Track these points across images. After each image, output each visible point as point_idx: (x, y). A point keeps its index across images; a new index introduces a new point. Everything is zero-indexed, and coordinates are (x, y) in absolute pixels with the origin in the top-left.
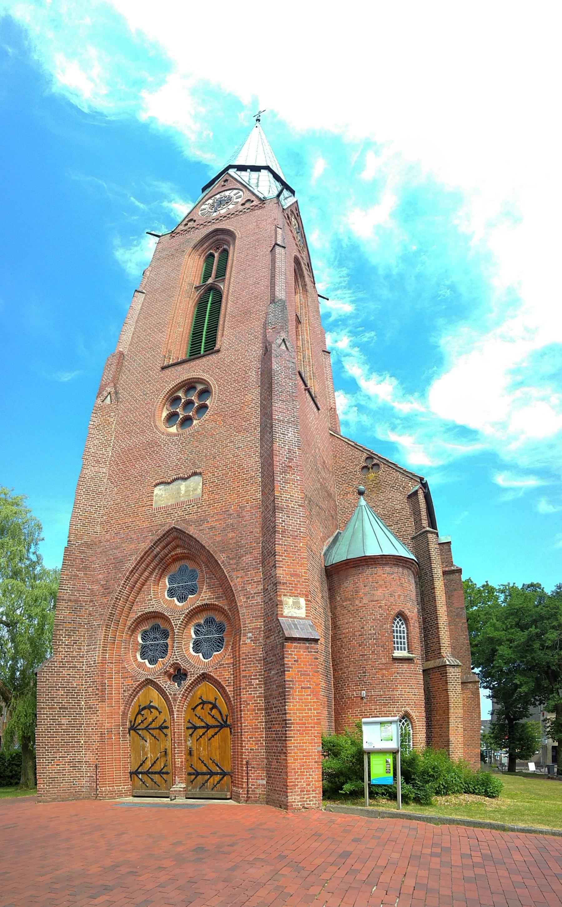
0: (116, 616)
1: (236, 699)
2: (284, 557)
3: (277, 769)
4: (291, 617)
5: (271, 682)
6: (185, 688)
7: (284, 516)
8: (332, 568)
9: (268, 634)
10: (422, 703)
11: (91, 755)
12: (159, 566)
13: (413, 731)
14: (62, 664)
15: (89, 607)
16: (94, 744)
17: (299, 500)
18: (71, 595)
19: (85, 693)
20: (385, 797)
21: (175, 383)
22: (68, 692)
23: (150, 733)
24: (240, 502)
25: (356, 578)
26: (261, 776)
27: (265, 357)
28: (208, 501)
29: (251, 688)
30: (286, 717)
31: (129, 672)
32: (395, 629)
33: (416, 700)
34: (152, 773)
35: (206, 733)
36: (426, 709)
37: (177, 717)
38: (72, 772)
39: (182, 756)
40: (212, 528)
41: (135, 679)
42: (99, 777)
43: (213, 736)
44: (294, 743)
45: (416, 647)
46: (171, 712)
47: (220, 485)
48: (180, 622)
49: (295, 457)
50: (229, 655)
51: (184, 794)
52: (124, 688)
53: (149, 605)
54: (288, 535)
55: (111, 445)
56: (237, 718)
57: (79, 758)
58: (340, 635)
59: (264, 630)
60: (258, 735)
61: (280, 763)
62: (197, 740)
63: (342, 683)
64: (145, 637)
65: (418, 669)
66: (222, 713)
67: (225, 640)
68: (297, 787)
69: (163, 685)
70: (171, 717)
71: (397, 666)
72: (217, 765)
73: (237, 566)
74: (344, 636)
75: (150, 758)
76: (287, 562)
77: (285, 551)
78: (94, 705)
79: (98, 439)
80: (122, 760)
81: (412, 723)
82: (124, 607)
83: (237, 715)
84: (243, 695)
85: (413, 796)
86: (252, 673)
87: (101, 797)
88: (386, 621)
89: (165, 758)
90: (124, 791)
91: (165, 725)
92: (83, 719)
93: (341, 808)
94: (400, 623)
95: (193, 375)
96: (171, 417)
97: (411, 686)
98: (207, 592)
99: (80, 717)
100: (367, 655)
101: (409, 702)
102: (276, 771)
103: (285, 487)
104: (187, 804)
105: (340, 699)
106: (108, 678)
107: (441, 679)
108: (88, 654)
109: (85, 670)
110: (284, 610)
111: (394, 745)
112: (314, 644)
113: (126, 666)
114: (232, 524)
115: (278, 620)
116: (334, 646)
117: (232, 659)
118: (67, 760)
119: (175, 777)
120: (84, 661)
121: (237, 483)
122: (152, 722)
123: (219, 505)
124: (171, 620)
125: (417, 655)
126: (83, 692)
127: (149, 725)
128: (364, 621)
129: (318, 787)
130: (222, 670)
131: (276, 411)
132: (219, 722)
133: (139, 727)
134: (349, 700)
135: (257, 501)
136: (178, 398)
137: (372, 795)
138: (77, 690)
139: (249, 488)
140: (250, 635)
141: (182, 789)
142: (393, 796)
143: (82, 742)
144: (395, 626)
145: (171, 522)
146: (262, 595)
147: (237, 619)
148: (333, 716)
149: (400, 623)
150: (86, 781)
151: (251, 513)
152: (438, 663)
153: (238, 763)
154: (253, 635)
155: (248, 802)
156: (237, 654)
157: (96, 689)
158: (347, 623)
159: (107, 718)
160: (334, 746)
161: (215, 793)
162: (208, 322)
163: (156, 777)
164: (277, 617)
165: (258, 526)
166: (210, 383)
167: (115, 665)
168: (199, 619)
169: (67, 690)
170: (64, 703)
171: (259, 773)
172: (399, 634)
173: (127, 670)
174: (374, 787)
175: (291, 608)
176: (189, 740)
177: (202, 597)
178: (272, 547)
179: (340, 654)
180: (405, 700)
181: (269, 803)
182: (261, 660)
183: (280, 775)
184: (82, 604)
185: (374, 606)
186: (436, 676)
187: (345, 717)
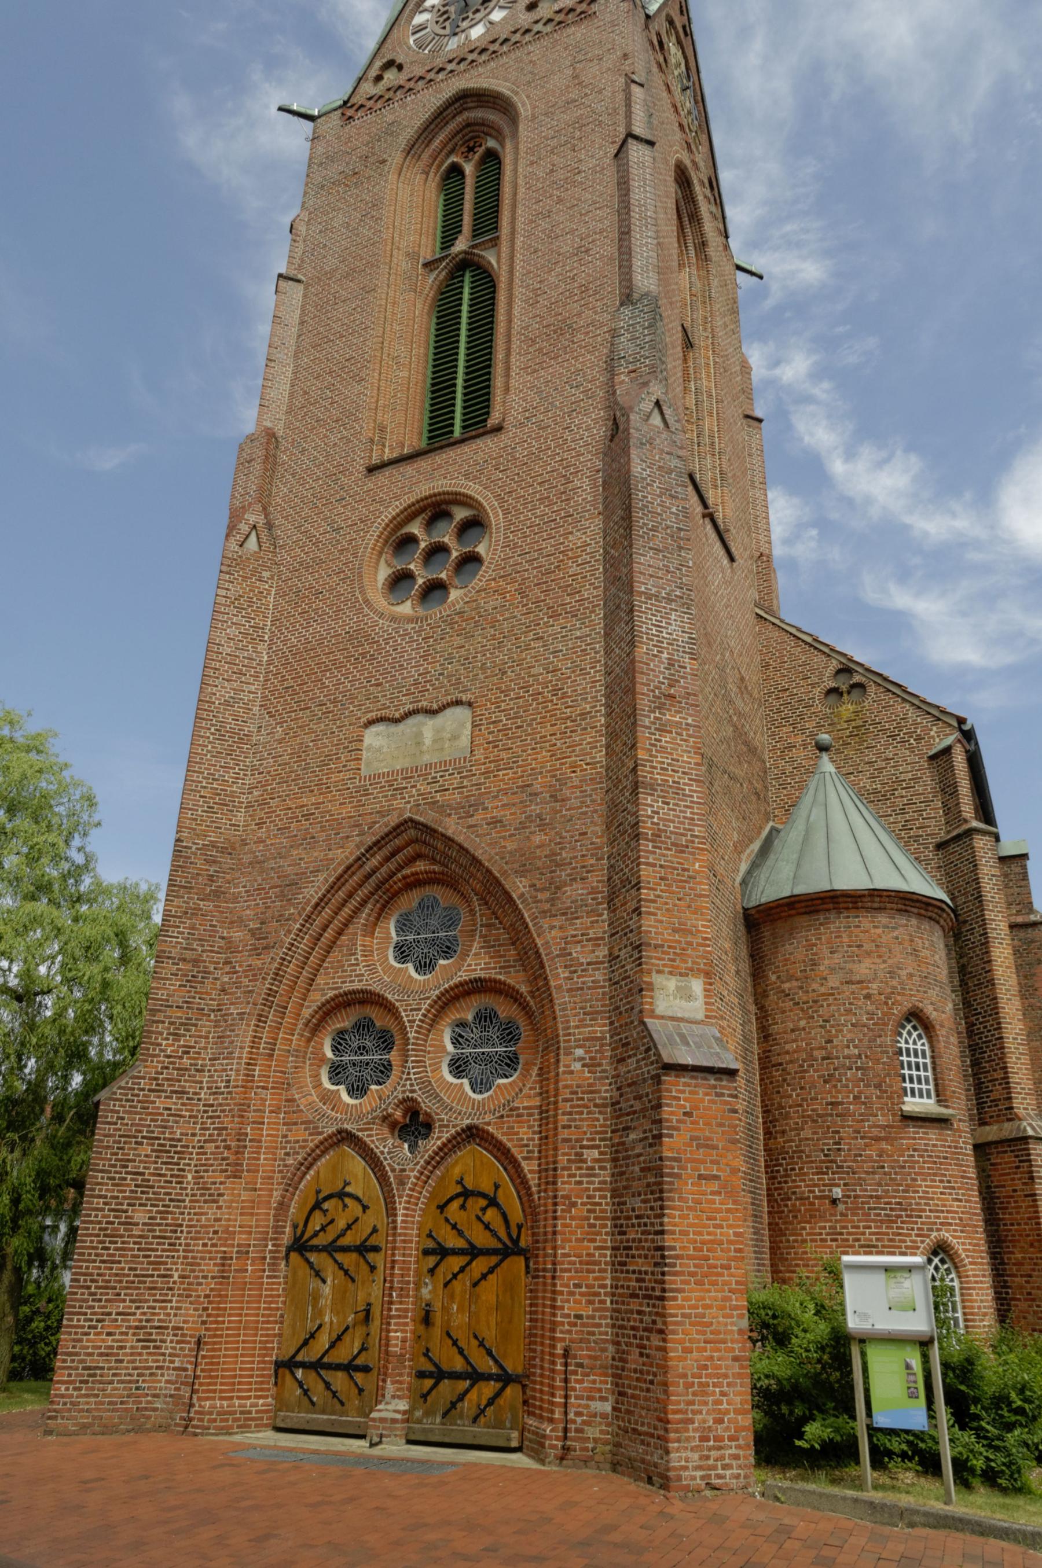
0: (281, 995)
1: (545, 1191)
2: (658, 893)
3: (641, 1372)
4: (672, 1019)
5: (628, 1157)
6: (426, 1157)
7: (658, 802)
8: (758, 912)
9: (621, 1053)
10: (977, 1221)
11: (191, 1312)
12: (376, 897)
13: (961, 1283)
14: (157, 1085)
15: (222, 974)
17: (692, 769)
18: (186, 949)
19: (198, 1154)
20: (910, 1465)
21: (401, 504)
23: (336, 1261)
24: (557, 770)
25: (813, 935)
26: (600, 1390)
27: (613, 446)
28: (485, 763)
29: (580, 1168)
30: (663, 1240)
31: (301, 1111)
32: (903, 1045)
33: (963, 1213)
34: (329, 1367)
35: (468, 1269)
36: (988, 1236)
37: (403, 1221)
38: (140, 1354)
39: (406, 1324)
40: (497, 822)
41: (314, 1128)
42: (202, 1370)
43: (484, 1277)
44: (683, 1307)
45: (954, 1092)
46: (391, 1212)
47: (511, 729)
48: (420, 1017)
49: (683, 677)
50: (531, 1089)
51: (403, 1428)
52: (286, 1148)
53: (351, 976)
54: (666, 843)
55: (266, 638)
56: (545, 1234)
57: (162, 1317)
58: (778, 1055)
59: (610, 1044)
61: (648, 1356)
62: (446, 1285)
63: (787, 1164)
64: (341, 1044)
65: (964, 1142)
66: (509, 1218)
67: (521, 1061)
68: (690, 1426)
69: (377, 1148)
70: (390, 1219)
71: (915, 1133)
72: (489, 1353)
73: (552, 905)
74: (787, 1057)
75: (328, 1326)
76: (666, 903)
77: (661, 878)
78: (215, 1183)
79: (236, 624)
80: (262, 1329)
81: (956, 1267)
82: (298, 978)
83: (545, 1226)
84: (563, 1183)
85: (979, 1464)
86: (585, 1133)
88: (882, 1030)
89: (364, 1328)
90: (257, 1412)
91: (372, 1242)
92: (183, 1213)
93: (803, 1492)
94: (915, 1034)
95: (442, 484)
96: (400, 579)
97: (949, 1182)
98: (480, 954)
99: (178, 1207)
100: (842, 1103)
101: (946, 1218)
102: (638, 1380)
103: (660, 741)
104: (413, 1461)
105: (782, 1200)
106: (254, 1122)
107: (1018, 1167)
108: (213, 1065)
109: (205, 1099)
110: (658, 1003)
111: (920, 1323)
112: (728, 1081)
113: (297, 1096)
114: (539, 816)
115: (644, 1024)
116: (768, 1081)
117: (538, 1099)
118: (134, 1321)
119: (384, 1381)
120: (205, 1080)
121: (552, 725)
123: (507, 774)
124: (401, 1009)
125: (958, 1109)
126: (195, 1151)
128: (832, 1026)
129: (744, 1428)
130: (514, 1122)
131: (641, 573)
132: (499, 1239)
134: (804, 1205)
135: (595, 768)
136: (410, 540)
137: (880, 1458)
138: (182, 1146)
139: (577, 739)
140: (579, 1052)
141: (399, 1416)
142: (930, 1465)
143: (176, 1278)
144: (903, 1041)
145: (403, 807)
146: (605, 968)
147: (549, 1015)
148: (766, 1238)
149: (915, 1034)
150: (167, 1382)
151: (581, 792)
152: (1007, 1130)
153: (542, 1352)
154: (586, 1052)
155: (565, 1462)
156: (552, 1086)
157: (226, 1147)
158: (793, 1031)
159: (241, 1214)
160: (774, 1317)
161: (480, 1432)
162: (470, 318)
163: (339, 1380)
164: (642, 1017)
165: (599, 821)
166: (485, 504)
167: (271, 1094)
168: (463, 1010)
169: (159, 1145)
171: (594, 1382)
172: (913, 1059)
173: (298, 1106)
174: (879, 1435)
175: (671, 998)
176: (426, 1284)
177: (469, 965)
178: (633, 868)
179: (781, 1098)
180: (937, 1211)
181: (620, 1469)
182: (604, 1106)
183: (648, 1390)
185: (853, 993)
186: (1006, 1159)
187: (796, 1241)
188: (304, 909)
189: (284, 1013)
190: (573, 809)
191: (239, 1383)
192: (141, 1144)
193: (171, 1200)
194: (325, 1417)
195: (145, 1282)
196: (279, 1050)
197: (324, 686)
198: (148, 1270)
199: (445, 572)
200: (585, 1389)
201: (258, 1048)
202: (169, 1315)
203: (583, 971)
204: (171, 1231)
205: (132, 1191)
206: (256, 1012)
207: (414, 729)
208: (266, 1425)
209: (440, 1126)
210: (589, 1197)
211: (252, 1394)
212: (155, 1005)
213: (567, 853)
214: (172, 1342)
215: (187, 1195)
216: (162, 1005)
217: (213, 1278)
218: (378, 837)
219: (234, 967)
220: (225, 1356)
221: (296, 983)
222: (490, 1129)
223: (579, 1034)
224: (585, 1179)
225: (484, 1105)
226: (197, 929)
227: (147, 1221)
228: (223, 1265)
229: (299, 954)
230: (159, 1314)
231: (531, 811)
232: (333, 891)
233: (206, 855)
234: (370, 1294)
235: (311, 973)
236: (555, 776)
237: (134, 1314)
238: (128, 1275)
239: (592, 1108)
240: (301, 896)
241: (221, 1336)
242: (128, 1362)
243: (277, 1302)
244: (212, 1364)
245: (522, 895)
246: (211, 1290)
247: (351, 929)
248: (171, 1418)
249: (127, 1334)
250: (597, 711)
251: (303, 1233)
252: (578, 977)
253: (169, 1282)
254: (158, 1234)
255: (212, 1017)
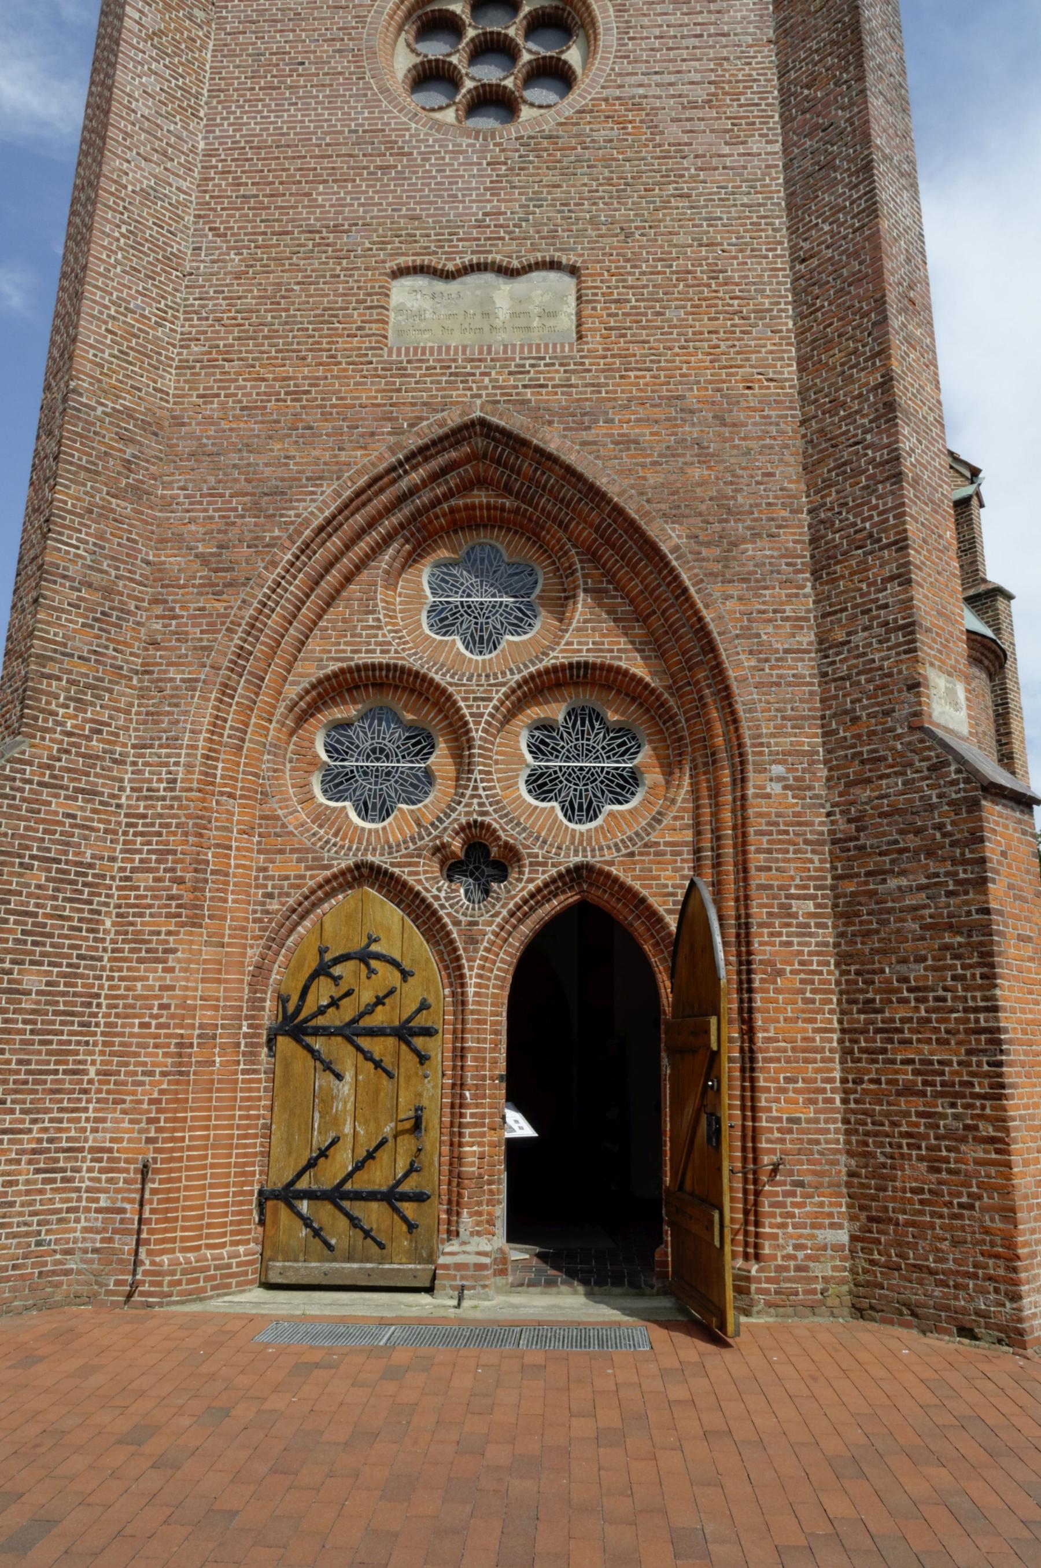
0: (257, 659)
11: (126, 1125)
15: (148, 618)
16: (142, 1083)
18: (91, 568)
22: (61, 880)
23: (359, 1049)
26: (830, 1215)
29: (789, 925)
31: (291, 833)
34: (358, 1196)
37: (476, 994)
38: (41, 1192)
40: (629, 442)
42: (153, 1211)
48: (490, 709)
50: (675, 818)
57: (73, 1134)
60: (817, 1071)
69: (427, 890)
73: (725, 567)
75: (350, 1139)
80: (238, 1146)
82: (283, 636)
84: (761, 944)
86: (793, 878)
87: (150, 1294)
90: (239, 1265)
91: (420, 1021)
92: (100, 978)
99: (92, 968)
106: (218, 846)
109: (129, 807)
113: (280, 812)
118: (29, 1141)
121: (709, 319)
122: (376, 1004)
124: (457, 697)
127: (361, 1015)
130: (651, 862)
133: (321, 1021)
138: (94, 876)
139: (752, 343)
140: (778, 770)
143: (92, 1074)
146: (811, 659)
150: (85, 1230)
154: (788, 770)
157: (173, 880)
159: (203, 980)
163: (374, 1214)
167: (240, 805)
169: (58, 871)
170: (45, 916)
171: (821, 1205)
182: (821, 843)
184: (125, 603)
188: (300, 533)
189: (260, 687)
190: (752, 439)
191: (209, 1226)
192: (30, 867)
193: (80, 957)
194: (355, 1266)
195: (45, 1082)
196: (251, 741)
197: (313, 205)
198: (48, 1063)
199: (512, 78)
200: (807, 1215)
201: (221, 735)
202: (83, 1130)
203: (777, 660)
204: (83, 1004)
205: (17, 941)
206: (219, 680)
207: (478, 293)
208: (251, 1282)
209: (531, 864)
210: (802, 963)
211: (227, 1239)
212: (45, 649)
213: (744, 497)
214: (90, 1170)
215: (105, 950)
216: (55, 651)
217: (163, 1074)
218: (426, 440)
219: (172, 609)
220: (187, 1188)
221: (279, 644)
222: (614, 870)
223: (777, 744)
224: (795, 940)
225: (590, 839)
226: (107, 540)
227: (43, 988)
228: (180, 1055)
229: (287, 600)
230: (68, 1130)
231: (684, 433)
232: (346, 512)
233: (119, 426)
234: (420, 1095)
235: (302, 633)
236: (719, 390)
237: (30, 1131)
238: (17, 1072)
239: (802, 846)
240: (292, 513)
241: (181, 1159)
242: (22, 1205)
243: (258, 1108)
244: (168, 1200)
245: (676, 549)
246: (162, 1092)
247: (365, 575)
248: (97, 1283)
249: (18, 1162)
250: (780, 310)
251: (299, 1009)
252: (771, 668)
253: (81, 1081)
254: (62, 1008)
255: (135, 682)
